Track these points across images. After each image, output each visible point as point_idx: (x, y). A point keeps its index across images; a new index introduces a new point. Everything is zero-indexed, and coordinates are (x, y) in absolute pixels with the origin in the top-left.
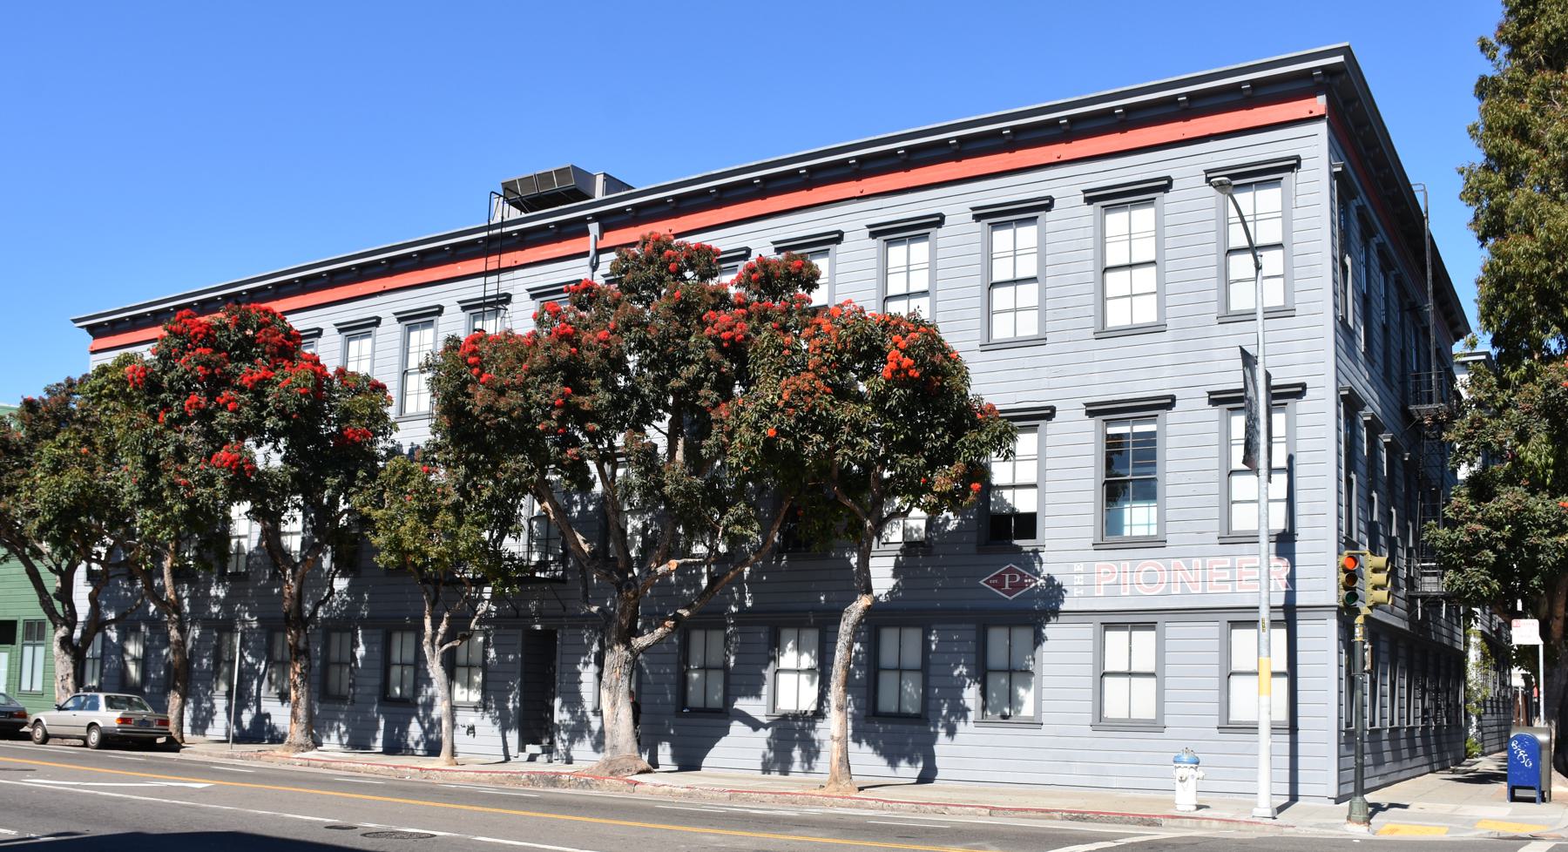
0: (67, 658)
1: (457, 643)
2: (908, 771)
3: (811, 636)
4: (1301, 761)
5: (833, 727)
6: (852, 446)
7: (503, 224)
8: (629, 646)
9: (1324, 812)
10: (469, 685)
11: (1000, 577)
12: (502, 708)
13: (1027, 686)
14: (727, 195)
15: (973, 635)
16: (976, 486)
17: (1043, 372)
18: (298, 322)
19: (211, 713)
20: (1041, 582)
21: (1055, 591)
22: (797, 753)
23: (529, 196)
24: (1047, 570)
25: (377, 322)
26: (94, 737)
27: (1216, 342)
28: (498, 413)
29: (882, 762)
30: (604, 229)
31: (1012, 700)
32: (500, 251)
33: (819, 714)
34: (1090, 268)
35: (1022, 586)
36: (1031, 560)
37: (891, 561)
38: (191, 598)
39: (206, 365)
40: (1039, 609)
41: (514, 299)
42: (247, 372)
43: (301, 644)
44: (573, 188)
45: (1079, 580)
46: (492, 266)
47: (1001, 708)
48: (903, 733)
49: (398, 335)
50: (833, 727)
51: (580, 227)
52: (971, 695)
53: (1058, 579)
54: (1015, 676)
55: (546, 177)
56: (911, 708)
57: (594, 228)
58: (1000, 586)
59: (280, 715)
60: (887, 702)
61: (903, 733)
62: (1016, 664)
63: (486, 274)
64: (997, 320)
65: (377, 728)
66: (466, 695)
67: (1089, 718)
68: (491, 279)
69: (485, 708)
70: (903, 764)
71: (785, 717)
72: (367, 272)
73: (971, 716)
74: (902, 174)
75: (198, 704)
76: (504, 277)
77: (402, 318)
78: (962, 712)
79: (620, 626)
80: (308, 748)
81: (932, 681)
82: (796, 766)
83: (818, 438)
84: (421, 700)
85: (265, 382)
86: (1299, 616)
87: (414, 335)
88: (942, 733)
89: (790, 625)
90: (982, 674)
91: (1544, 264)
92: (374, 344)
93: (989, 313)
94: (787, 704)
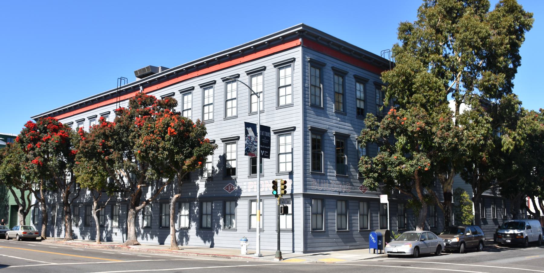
0: (22, 216)
1: (100, 209)
2: (208, 244)
3: (188, 205)
4: (276, 240)
5: (192, 232)
6: (162, 154)
7: (120, 88)
8: (134, 209)
9: (297, 257)
10: (116, 221)
11: (228, 187)
12: (123, 228)
13: (234, 219)
14: (210, 64)
15: (221, 204)
16: (200, 163)
17: (237, 126)
18: (63, 122)
19: (61, 230)
20: (237, 188)
21: (240, 190)
22: (184, 239)
23: (142, 74)
24: (238, 184)
25: (193, 88)
26: (18, 238)
27: (276, 115)
28: (85, 148)
29: (202, 241)
30: (144, 88)
31: (231, 223)
32: (120, 96)
33: (189, 228)
34: (200, 105)
35: (232, 189)
36: (234, 181)
37: (204, 183)
38: (57, 197)
39: (33, 135)
40: (235, 196)
41: (217, 82)
42: (44, 136)
43: (68, 210)
44: (152, 70)
45: (245, 187)
46: (118, 100)
47: (228, 225)
48: (207, 233)
49: (223, 87)
50: (192, 232)
51: (137, 88)
52: (221, 222)
53: (241, 187)
54: (232, 216)
55: (144, 69)
56: (209, 226)
57: (141, 88)
58: (227, 190)
59: (77, 231)
60: (204, 225)
61: (207, 233)
62: (232, 212)
63: (117, 102)
64: (281, 99)
65: (96, 234)
66: (116, 224)
67: (247, 228)
68: (118, 104)
69: (119, 227)
70: (207, 242)
71: (182, 229)
72: (161, 80)
73: (222, 228)
74: (254, 54)
75: (58, 228)
76: (121, 103)
77: (276, 65)
78: (219, 226)
79: (132, 204)
80: (70, 240)
81: (213, 218)
82: (184, 243)
83: (153, 152)
84: (105, 225)
85: (48, 139)
86: (294, 197)
87: (186, 97)
88: (215, 232)
89: (228, 201)
90: (224, 216)
91: (396, 78)
92: (214, 91)
93: (226, 109)
94: (183, 225)
